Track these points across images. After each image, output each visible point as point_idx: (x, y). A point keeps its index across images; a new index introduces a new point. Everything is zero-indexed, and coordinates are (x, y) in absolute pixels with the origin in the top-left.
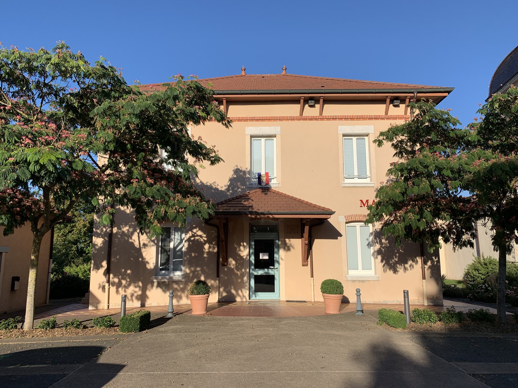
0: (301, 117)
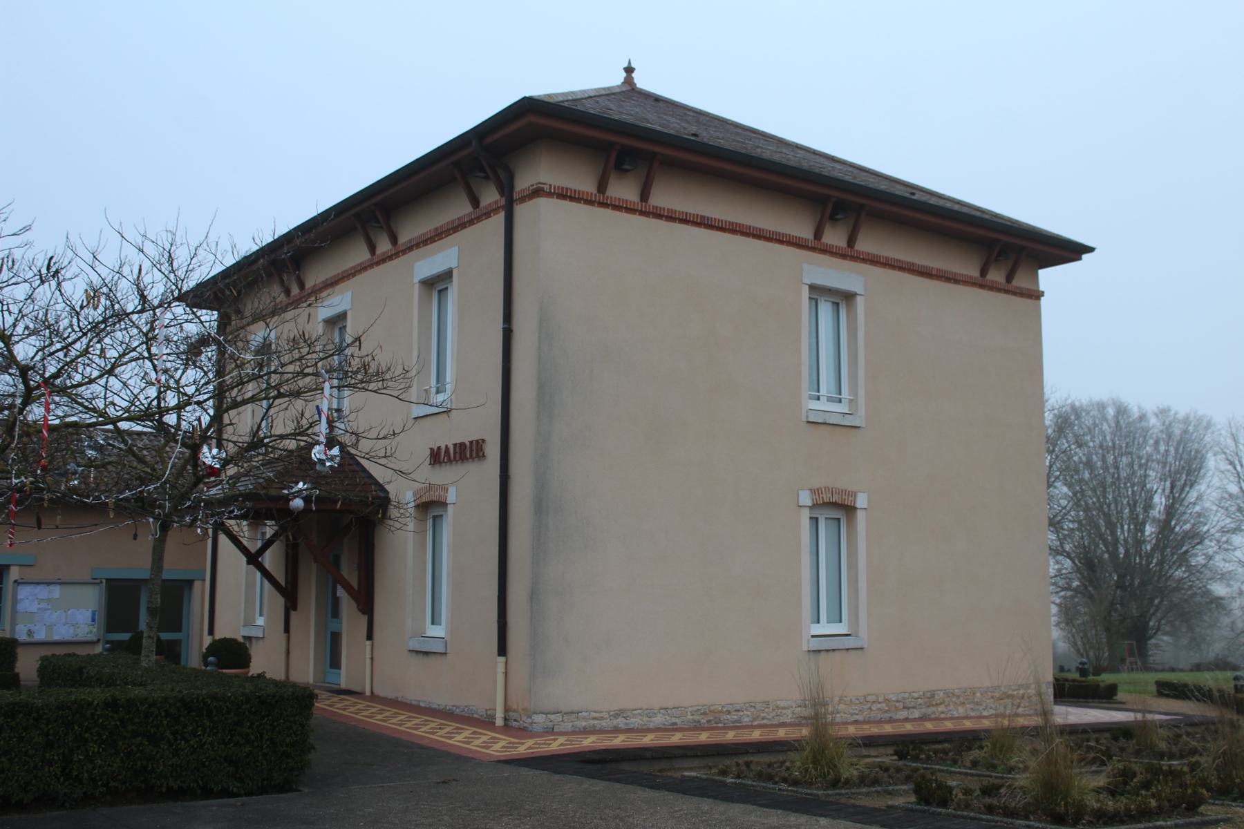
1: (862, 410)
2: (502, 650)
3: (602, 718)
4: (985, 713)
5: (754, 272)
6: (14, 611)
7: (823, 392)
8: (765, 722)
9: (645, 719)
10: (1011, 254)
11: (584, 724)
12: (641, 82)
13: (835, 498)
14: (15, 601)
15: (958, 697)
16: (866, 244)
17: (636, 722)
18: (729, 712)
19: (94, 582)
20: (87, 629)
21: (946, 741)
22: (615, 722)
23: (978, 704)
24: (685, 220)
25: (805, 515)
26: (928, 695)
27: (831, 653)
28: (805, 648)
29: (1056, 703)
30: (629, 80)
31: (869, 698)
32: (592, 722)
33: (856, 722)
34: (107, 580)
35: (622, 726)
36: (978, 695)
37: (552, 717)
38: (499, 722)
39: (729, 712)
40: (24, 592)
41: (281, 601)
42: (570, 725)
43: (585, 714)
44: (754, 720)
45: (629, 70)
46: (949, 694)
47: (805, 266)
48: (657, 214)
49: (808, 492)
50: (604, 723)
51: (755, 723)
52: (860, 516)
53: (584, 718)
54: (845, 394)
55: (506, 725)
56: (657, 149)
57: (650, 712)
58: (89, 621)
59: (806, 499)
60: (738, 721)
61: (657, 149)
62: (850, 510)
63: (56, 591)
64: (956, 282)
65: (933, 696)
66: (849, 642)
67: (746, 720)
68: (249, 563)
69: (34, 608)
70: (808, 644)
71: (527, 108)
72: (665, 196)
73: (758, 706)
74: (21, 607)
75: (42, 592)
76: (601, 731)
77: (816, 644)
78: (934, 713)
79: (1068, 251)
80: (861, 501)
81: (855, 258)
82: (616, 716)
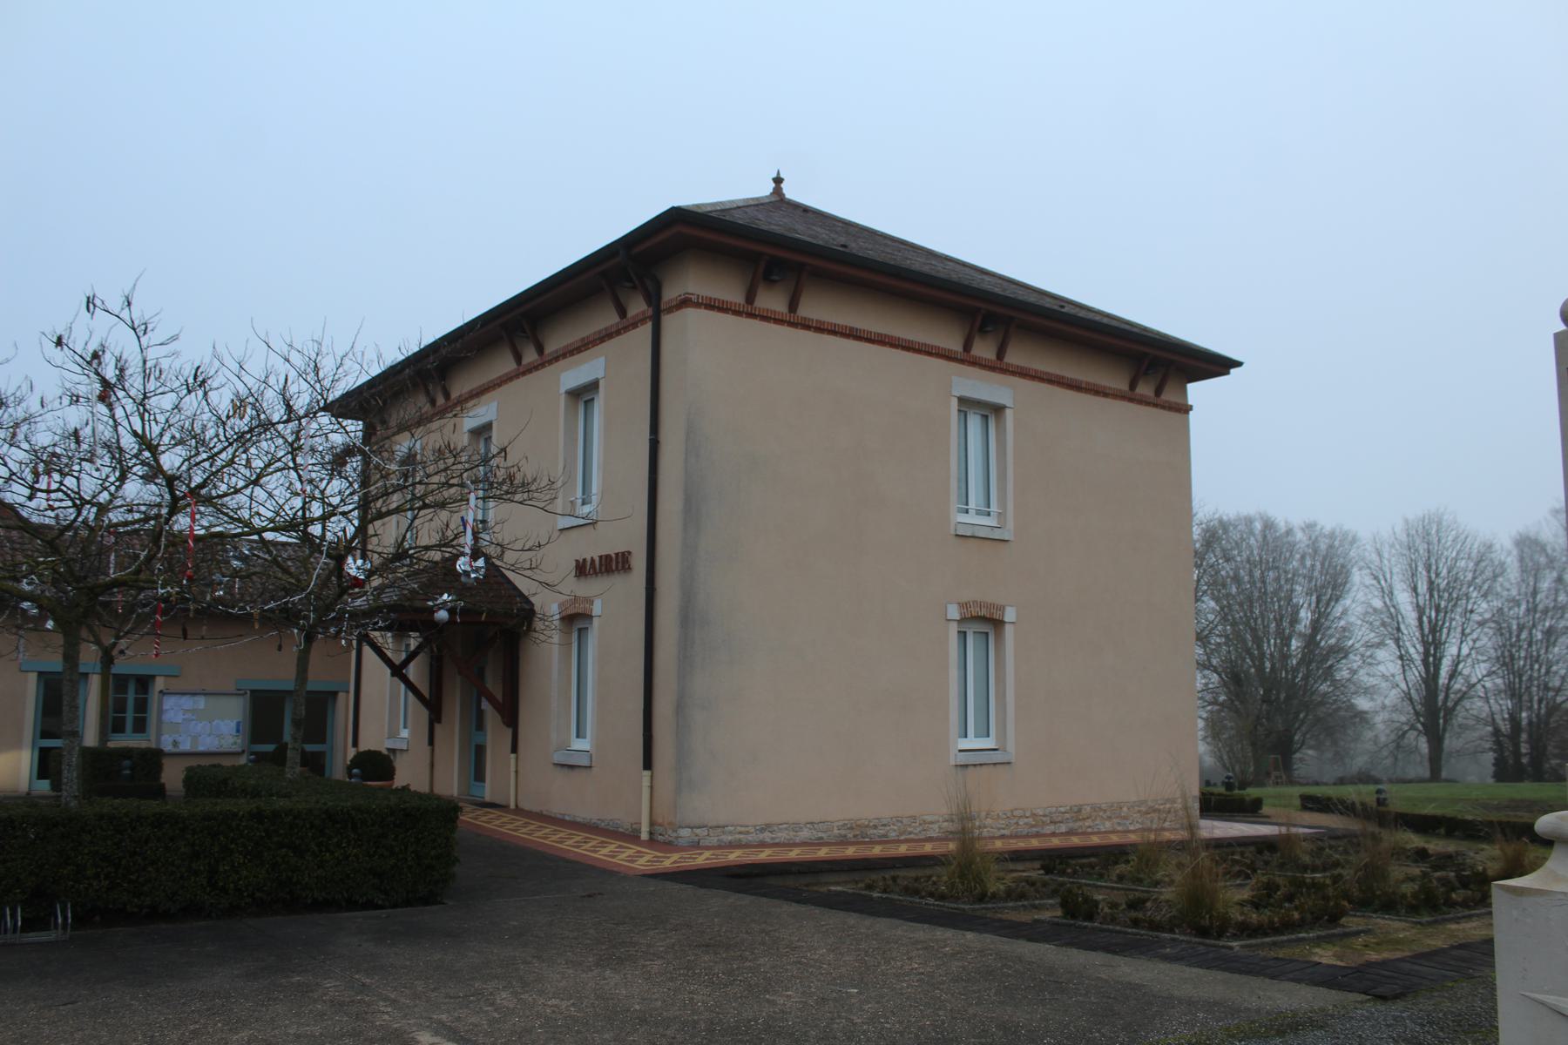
1: (1010, 524)
2: (648, 764)
3: (748, 833)
5: (901, 384)
6: (160, 721)
7: (972, 505)
10: (1161, 367)
14: (161, 712)
17: (782, 836)
18: (875, 827)
19: (239, 693)
22: (761, 836)
23: (1125, 818)
24: (834, 331)
25: (953, 629)
28: (953, 763)
29: (1202, 817)
33: (1003, 837)
37: (698, 831)
38: (644, 836)
39: (875, 827)
40: (169, 702)
41: (424, 714)
48: (805, 325)
52: (1009, 631)
54: (994, 508)
57: (796, 827)
59: (954, 612)
60: (885, 836)
62: (998, 624)
63: (201, 702)
64: (1106, 395)
65: (1080, 811)
67: (893, 835)
69: (179, 718)
70: (955, 758)
71: (676, 218)
72: (814, 307)
74: (167, 717)
75: (187, 702)
80: (1010, 615)
82: (762, 830)
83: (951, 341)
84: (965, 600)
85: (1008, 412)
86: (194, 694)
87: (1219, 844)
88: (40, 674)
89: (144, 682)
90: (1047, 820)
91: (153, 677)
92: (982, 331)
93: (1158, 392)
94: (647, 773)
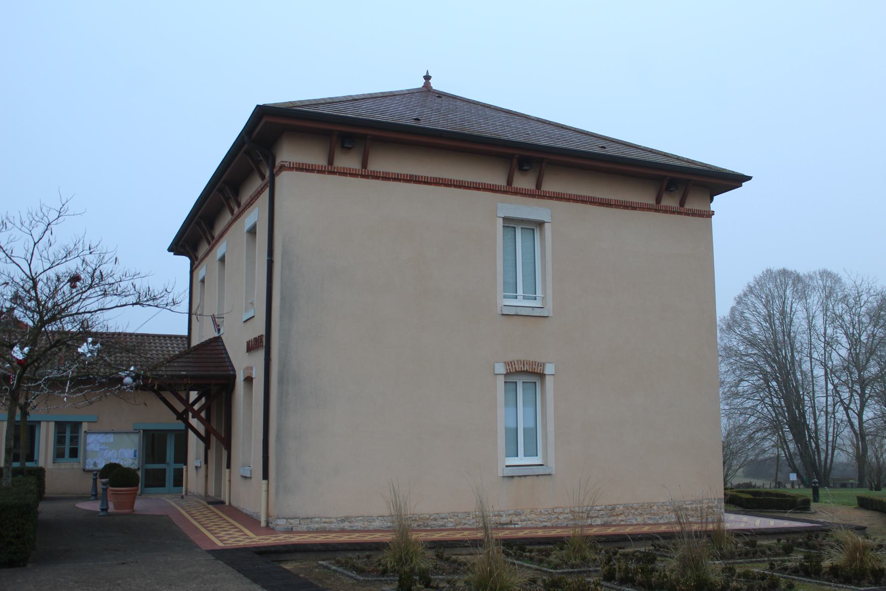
0: (330, 170)
1: (550, 305)
2: (266, 476)
3: (331, 523)
4: (661, 521)
5: (464, 214)
6: (85, 451)
7: (520, 292)
8: (467, 526)
9: (366, 523)
10: (686, 186)
11: (317, 526)
12: (435, 85)
13: (527, 368)
14: (85, 444)
15: (637, 509)
16: (551, 185)
17: (359, 525)
18: (435, 520)
19: (136, 431)
20: (131, 461)
21: (549, 543)
22: (342, 525)
23: (654, 514)
24: (397, 178)
25: (501, 380)
26: (610, 508)
27: (523, 478)
28: (500, 474)
29: (726, 511)
30: (427, 85)
31: (556, 510)
32: (322, 525)
33: (545, 527)
34: (144, 431)
35: (347, 528)
36: (655, 508)
37: (292, 521)
38: (263, 524)
39: (435, 520)
40: (91, 438)
41: (202, 445)
42: (305, 527)
43: (317, 519)
44: (457, 525)
45: (427, 78)
46: (626, 507)
47: (499, 205)
48: (375, 176)
49: (502, 365)
50: (332, 526)
51: (458, 527)
52: (549, 380)
53: (317, 522)
54: (539, 293)
55: (267, 526)
56: (370, 132)
57: (370, 519)
58: (133, 457)
59: (501, 369)
60: (444, 526)
61: (370, 132)
62: (542, 376)
63: (111, 438)
64: (634, 208)
65: (613, 509)
66: (540, 471)
67: (450, 525)
68: (178, 419)
69: (97, 449)
70: (502, 471)
71: (262, 113)
72: (380, 163)
73: (460, 515)
74: (89, 448)
75: (101, 438)
76: (331, 531)
77: (509, 472)
78: (614, 521)
79: (732, 181)
80: (549, 369)
81: (543, 196)
82: (343, 521)
83: (318, 159)
84: (509, 359)
85: (547, 226)
86: (107, 433)
87: (739, 533)
88: (57, 423)
89: (76, 426)
90: (585, 515)
91: (81, 423)
92: (346, 149)
93: (682, 204)
94: (265, 482)
